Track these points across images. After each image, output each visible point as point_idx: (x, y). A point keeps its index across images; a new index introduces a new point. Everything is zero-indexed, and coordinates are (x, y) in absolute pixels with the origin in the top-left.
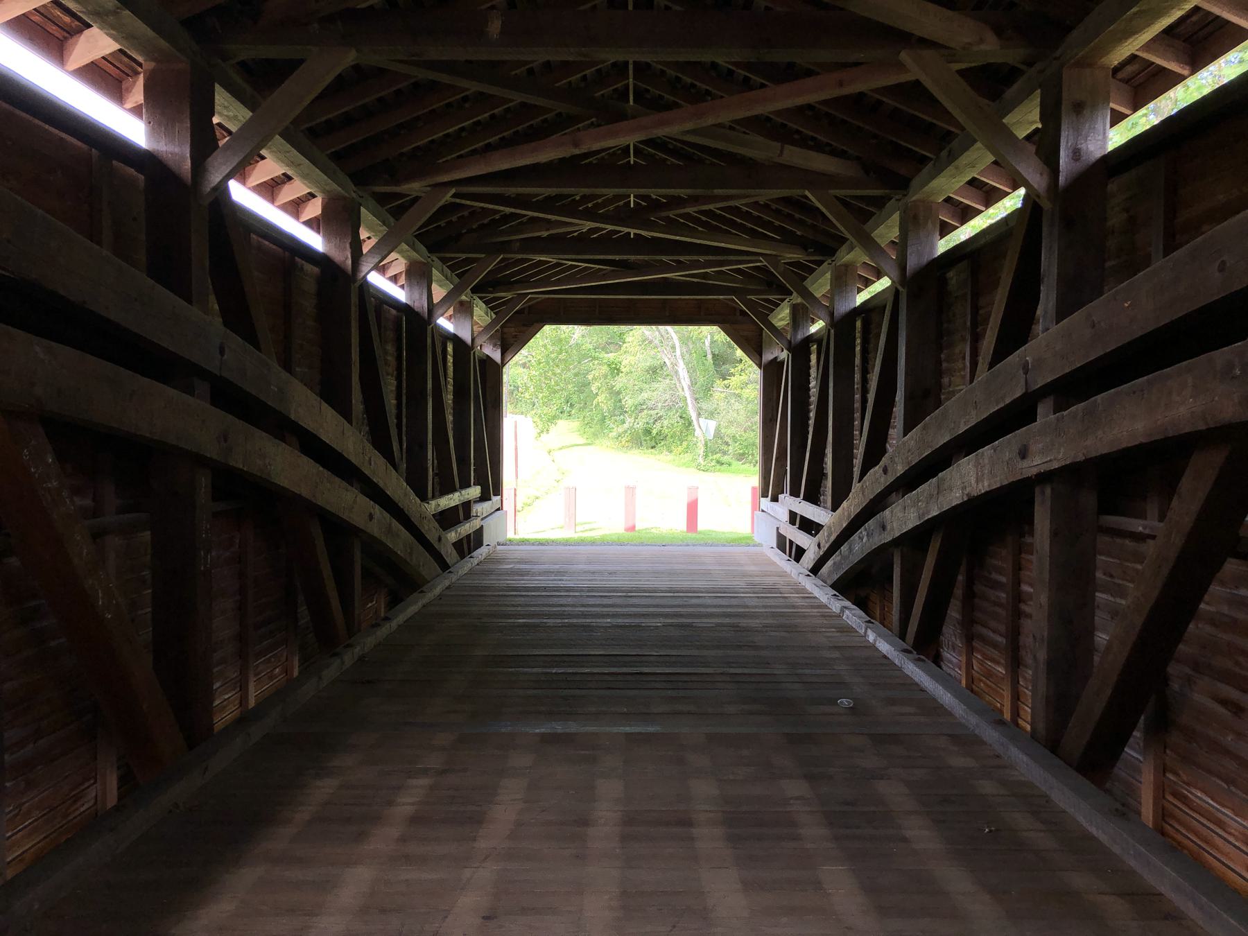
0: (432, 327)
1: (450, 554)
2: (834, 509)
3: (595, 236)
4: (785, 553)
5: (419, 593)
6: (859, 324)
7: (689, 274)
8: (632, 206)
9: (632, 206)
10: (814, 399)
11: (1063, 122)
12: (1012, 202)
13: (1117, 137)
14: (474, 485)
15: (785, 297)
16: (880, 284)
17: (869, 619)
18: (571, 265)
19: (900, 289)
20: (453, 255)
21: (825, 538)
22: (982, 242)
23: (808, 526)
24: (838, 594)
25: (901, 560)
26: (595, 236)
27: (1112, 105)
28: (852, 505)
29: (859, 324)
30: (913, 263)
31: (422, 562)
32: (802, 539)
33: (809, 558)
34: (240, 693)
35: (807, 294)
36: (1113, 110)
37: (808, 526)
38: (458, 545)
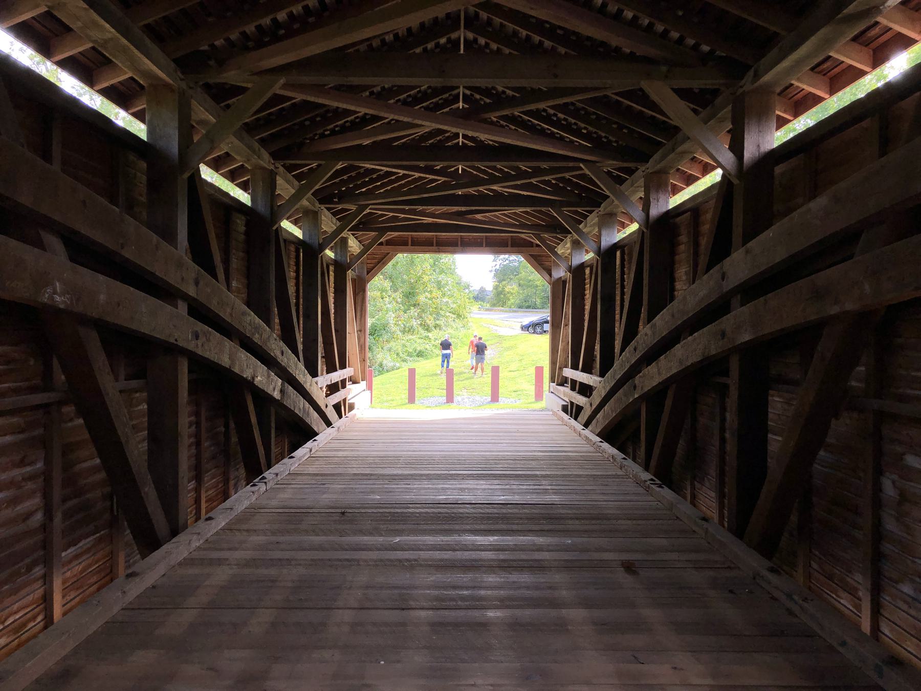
0: (322, 256)
1: (331, 414)
2: (602, 375)
3: (405, 189)
4: (567, 414)
5: (252, 486)
6: (618, 253)
7: (415, 221)
8: (460, 172)
9: (460, 172)
10: (588, 307)
11: (745, 128)
12: (716, 176)
13: (780, 137)
14: (340, 369)
15: (567, 235)
16: (795, 130)
17: (625, 457)
18: (381, 214)
19: (645, 230)
20: (552, 211)
21: (597, 398)
22: (700, 200)
23: (585, 390)
24: (603, 441)
25: (649, 464)
26: (405, 189)
27: (778, 112)
28: (619, 368)
29: (618, 253)
30: (655, 212)
31: (314, 419)
32: (580, 400)
33: (584, 416)
34: (224, 487)
35: (579, 232)
36: (779, 117)
37: (585, 390)
38: (337, 407)
